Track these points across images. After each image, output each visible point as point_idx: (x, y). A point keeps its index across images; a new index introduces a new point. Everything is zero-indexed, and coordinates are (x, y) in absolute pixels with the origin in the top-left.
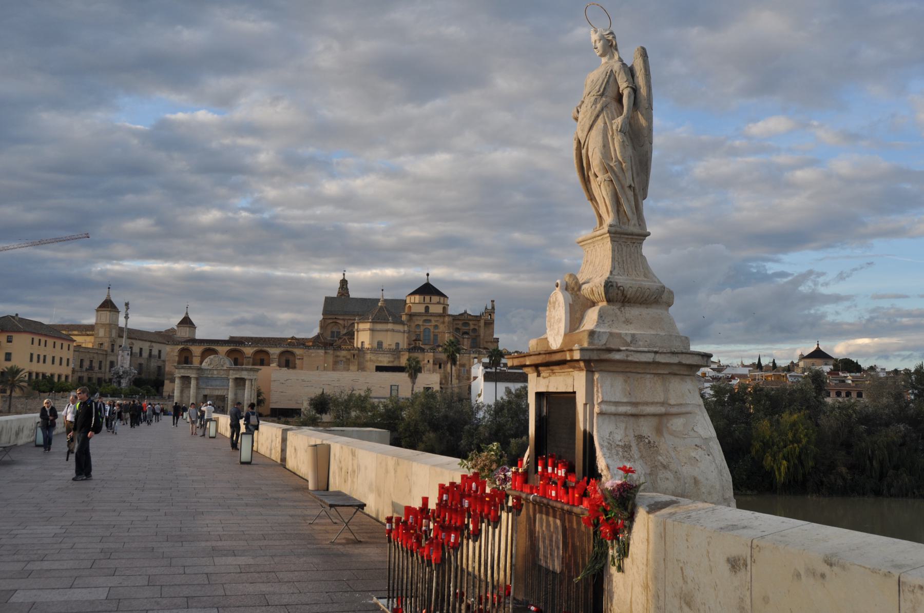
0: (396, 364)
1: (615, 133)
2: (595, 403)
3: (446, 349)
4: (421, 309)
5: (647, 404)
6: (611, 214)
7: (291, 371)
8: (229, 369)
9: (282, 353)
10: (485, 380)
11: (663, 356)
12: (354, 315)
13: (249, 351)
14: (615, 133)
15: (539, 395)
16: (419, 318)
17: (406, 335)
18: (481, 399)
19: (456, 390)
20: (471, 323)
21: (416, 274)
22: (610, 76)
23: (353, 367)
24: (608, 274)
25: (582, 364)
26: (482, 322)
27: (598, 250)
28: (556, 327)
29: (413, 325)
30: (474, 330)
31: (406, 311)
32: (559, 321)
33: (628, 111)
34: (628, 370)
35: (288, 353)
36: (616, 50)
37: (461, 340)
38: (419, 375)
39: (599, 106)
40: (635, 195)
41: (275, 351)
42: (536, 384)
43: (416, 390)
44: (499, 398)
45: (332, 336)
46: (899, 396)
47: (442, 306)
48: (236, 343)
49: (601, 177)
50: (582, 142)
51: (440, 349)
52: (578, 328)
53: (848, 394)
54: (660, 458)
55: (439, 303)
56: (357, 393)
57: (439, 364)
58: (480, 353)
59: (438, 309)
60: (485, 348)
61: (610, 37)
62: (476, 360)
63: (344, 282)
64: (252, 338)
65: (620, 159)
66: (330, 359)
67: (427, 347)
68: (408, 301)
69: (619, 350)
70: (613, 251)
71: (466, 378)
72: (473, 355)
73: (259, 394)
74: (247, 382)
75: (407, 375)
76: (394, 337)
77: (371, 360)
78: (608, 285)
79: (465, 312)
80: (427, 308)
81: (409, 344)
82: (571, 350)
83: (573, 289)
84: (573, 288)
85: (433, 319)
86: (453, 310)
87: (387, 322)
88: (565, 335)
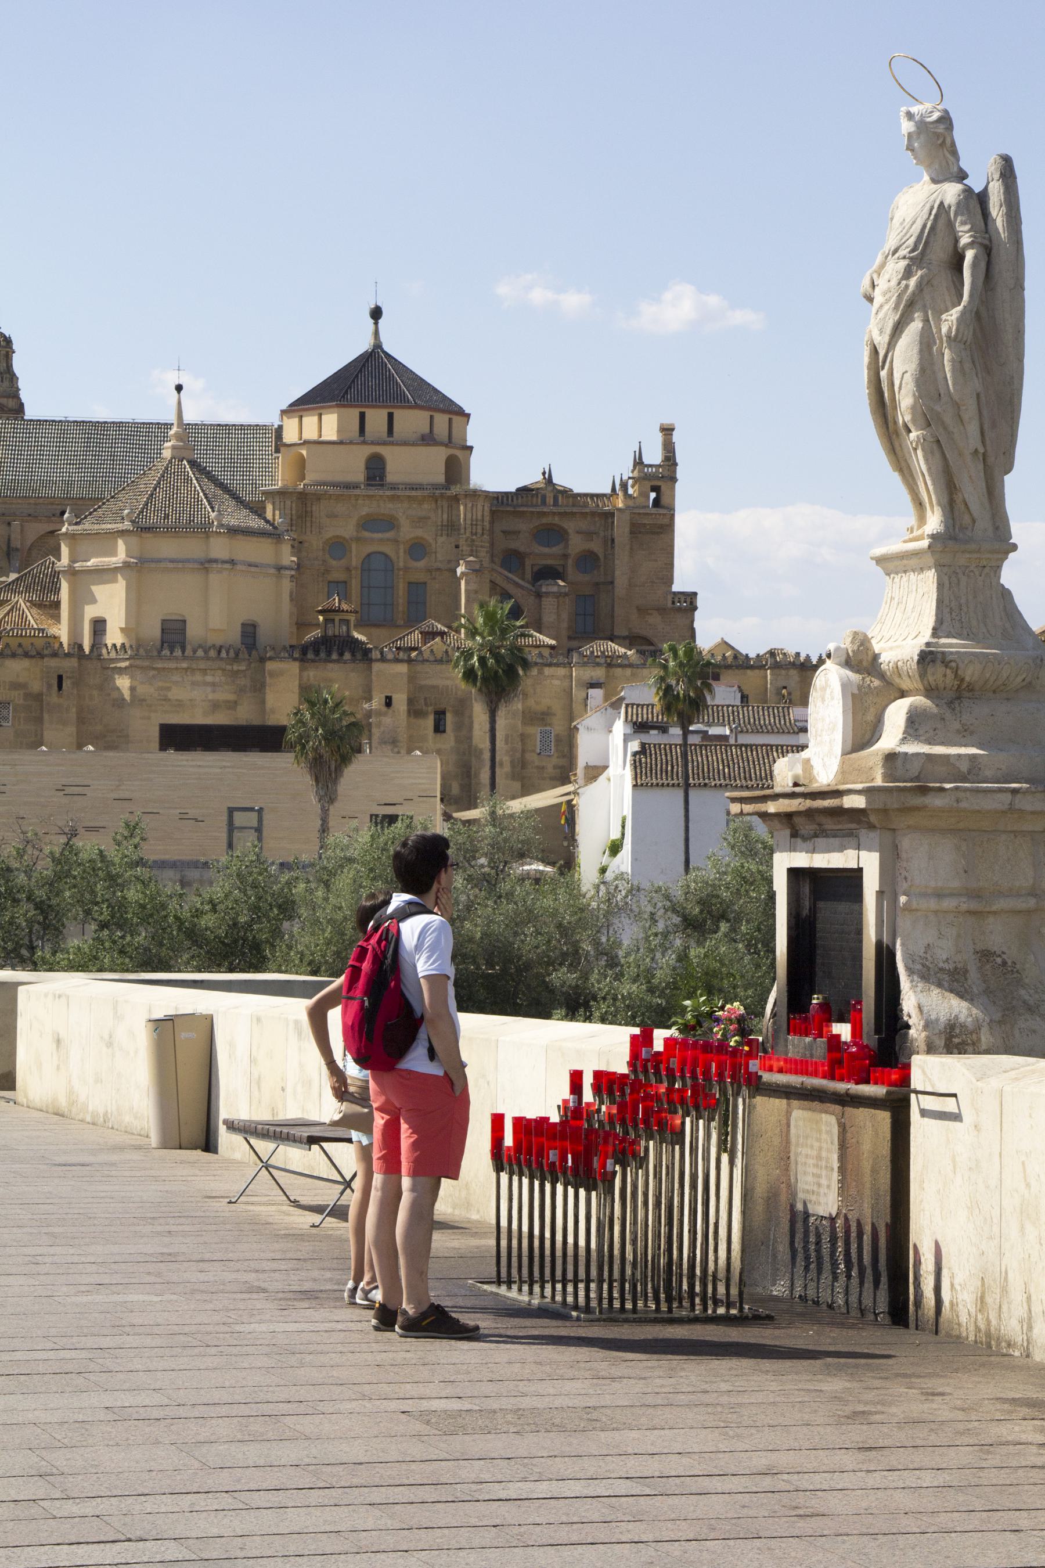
0: (244, 715)
15: (795, 874)
17: (287, 585)
20: (570, 526)
24: (926, 636)
30: (588, 560)
33: (971, 296)
54: (1023, 992)
55: (428, 439)
56: (87, 846)
80: (376, 469)
85: (401, 512)
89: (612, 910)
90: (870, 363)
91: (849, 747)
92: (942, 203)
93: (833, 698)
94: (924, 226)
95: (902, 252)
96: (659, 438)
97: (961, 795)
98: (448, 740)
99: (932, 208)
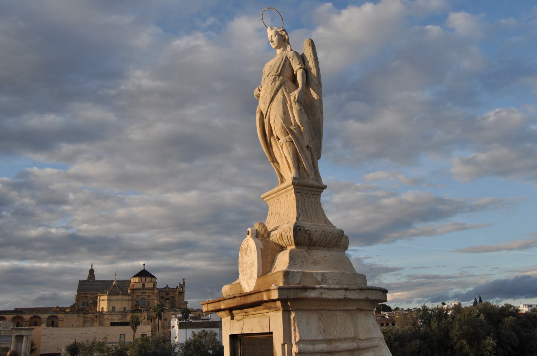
0: (124, 321)
1: (293, 103)
2: (293, 342)
3: (155, 310)
4: (140, 286)
5: (339, 340)
6: (293, 171)
7: (55, 328)
8: (13, 330)
9: (50, 317)
10: (179, 328)
11: (353, 292)
12: (98, 291)
13: (27, 317)
14: (293, 103)
15: (233, 338)
16: (138, 291)
17: (130, 302)
18: (177, 340)
19: (162, 335)
20: (170, 293)
21: (139, 264)
22: (285, 61)
23: (96, 324)
24: (294, 221)
25: (279, 304)
26: (177, 292)
27: (282, 202)
28: (248, 271)
29: (135, 296)
30: (173, 297)
31: (131, 287)
32: (252, 265)
33: (303, 85)
34: (321, 308)
35: (53, 317)
36: (289, 43)
37: (164, 303)
38: (138, 327)
39: (278, 83)
40: (312, 155)
41: (44, 316)
42: (230, 327)
43: (136, 337)
44: (188, 339)
45: (83, 305)
46: (415, 324)
47: (152, 284)
48: (19, 312)
49: (282, 139)
50: (264, 114)
51: (152, 310)
52: (270, 271)
53: (387, 324)
55: (151, 282)
56: (98, 341)
57: (151, 319)
58: (176, 311)
59: (150, 285)
60: (179, 308)
61: (284, 33)
62: (174, 316)
63: (92, 271)
64: (30, 309)
65: (299, 124)
66: (81, 320)
67: (143, 309)
68: (132, 281)
69: (314, 289)
70: (297, 201)
71: (168, 326)
72: (172, 313)
73: (32, 345)
74: (24, 338)
75: (130, 327)
76: (123, 303)
77: (108, 319)
78: (297, 229)
79: (167, 286)
80: (144, 285)
81: (132, 308)
82: (269, 290)
83: (263, 235)
84: (263, 237)
85: (146, 291)
86: (159, 286)
87: (118, 294)
88: (258, 277)
89: (175, 346)
90: (260, 118)
91: (261, 274)
92: (286, 57)
93: (251, 252)
94: (280, 64)
95: (271, 74)
96: (182, 280)
97: (323, 291)
98: (153, 323)
99: (283, 58)
